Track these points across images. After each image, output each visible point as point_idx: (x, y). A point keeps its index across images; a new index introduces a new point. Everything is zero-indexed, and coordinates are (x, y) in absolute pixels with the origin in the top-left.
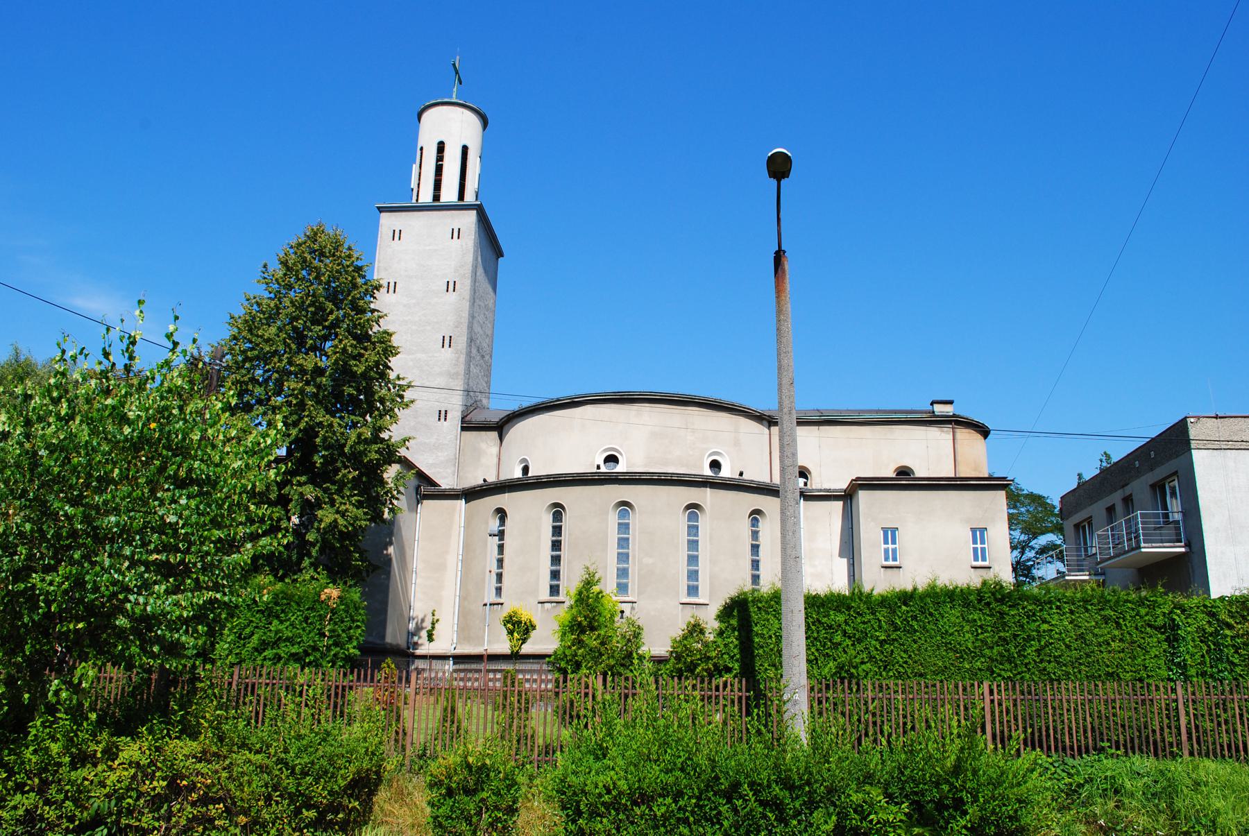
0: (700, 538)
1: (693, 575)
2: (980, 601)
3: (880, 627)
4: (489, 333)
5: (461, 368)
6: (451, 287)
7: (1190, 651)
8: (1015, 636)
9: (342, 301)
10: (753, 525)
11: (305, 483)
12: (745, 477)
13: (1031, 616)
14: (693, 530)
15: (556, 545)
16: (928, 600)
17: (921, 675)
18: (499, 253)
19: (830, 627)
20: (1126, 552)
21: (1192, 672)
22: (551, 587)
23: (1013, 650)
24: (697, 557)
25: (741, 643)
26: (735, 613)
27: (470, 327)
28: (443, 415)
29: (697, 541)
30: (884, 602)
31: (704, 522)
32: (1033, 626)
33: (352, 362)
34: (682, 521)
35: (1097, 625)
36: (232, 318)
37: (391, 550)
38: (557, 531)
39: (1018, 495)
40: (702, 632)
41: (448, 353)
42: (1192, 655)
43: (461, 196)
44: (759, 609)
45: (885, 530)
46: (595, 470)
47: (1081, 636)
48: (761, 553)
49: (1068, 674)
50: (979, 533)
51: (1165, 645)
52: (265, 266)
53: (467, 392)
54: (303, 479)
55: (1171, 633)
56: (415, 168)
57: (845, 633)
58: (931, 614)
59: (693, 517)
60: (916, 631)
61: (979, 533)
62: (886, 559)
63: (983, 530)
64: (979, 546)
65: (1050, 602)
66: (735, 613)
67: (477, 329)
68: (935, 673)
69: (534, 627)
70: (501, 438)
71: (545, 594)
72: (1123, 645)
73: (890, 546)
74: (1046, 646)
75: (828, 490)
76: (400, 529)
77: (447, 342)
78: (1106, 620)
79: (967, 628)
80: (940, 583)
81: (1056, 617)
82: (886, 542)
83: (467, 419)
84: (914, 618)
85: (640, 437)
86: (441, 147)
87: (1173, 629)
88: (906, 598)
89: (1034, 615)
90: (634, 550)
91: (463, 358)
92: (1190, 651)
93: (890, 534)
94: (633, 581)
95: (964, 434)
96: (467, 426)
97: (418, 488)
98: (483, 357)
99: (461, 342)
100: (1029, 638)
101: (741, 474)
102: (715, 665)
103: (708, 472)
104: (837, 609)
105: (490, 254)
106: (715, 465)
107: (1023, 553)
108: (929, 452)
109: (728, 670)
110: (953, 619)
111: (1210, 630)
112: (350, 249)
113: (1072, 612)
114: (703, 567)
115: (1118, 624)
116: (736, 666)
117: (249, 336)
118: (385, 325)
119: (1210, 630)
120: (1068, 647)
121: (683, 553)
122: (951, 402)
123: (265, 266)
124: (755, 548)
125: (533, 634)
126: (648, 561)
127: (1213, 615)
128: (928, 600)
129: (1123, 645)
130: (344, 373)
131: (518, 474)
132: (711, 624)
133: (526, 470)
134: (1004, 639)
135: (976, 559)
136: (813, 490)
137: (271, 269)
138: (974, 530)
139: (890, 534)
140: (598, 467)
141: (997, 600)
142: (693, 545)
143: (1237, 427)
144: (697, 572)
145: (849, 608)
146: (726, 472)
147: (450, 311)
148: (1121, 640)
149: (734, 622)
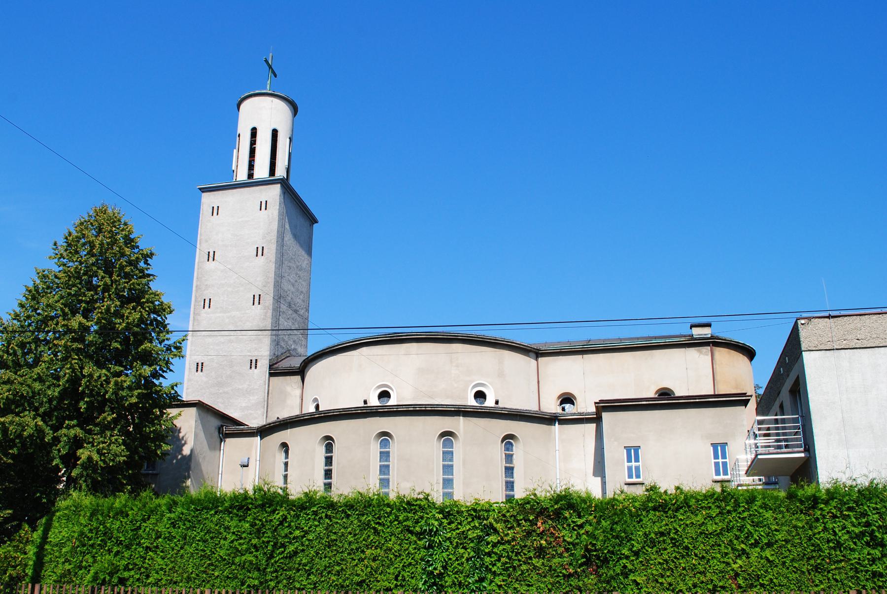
0: (377, 464)
4: (304, 290)
6: (260, 252)
10: (507, 449)
11: (74, 426)
12: (500, 405)
14: (448, 455)
18: (312, 220)
27: (278, 285)
28: (254, 364)
29: (452, 466)
31: (458, 448)
34: (437, 448)
37: (189, 482)
38: (329, 461)
41: (258, 309)
43: (272, 171)
45: (628, 449)
46: (362, 405)
50: (719, 449)
52: (55, 244)
54: (75, 422)
56: (235, 151)
59: (448, 444)
61: (719, 449)
62: (630, 476)
63: (724, 445)
64: (720, 460)
67: (286, 286)
73: (633, 464)
75: (580, 414)
76: (198, 465)
82: (629, 460)
85: (408, 373)
86: (254, 132)
93: (633, 452)
95: (722, 354)
96: (275, 371)
97: (220, 429)
99: (268, 300)
105: (302, 221)
108: (688, 372)
112: (126, 224)
123: (55, 244)
131: (312, 409)
133: (317, 407)
139: (633, 452)
143: (852, 326)
146: (490, 403)
147: (260, 273)
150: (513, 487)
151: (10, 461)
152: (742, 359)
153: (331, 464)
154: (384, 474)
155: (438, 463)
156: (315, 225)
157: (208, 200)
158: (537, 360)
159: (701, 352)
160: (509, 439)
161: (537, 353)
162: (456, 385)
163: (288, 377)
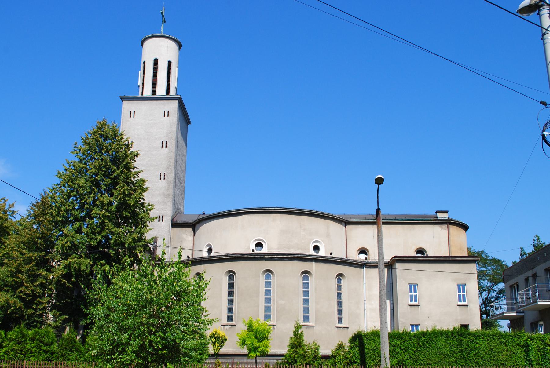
0: (310, 289)
1: (306, 310)
2: (452, 335)
3: (414, 346)
4: (184, 169)
5: (171, 192)
6: (164, 144)
7: (534, 355)
8: (466, 349)
9: (119, 165)
10: (338, 282)
12: (334, 255)
13: (472, 341)
14: (306, 285)
15: (231, 294)
16: (432, 335)
17: (430, 364)
19: (395, 346)
20: (531, 304)
21: (534, 363)
22: (228, 317)
23: (465, 354)
24: (308, 300)
25: (360, 352)
26: (357, 340)
27: (176, 168)
29: (308, 291)
30: (415, 336)
31: (312, 281)
32: (473, 345)
33: (127, 198)
34: (300, 281)
35: (498, 345)
36: (59, 173)
38: (231, 286)
39: (486, 260)
40: (344, 347)
42: (535, 357)
44: (367, 338)
45: (410, 285)
47: (491, 349)
48: (342, 298)
49: (486, 364)
50: (461, 287)
51: (524, 353)
52: (76, 144)
53: (174, 205)
54: (103, 262)
55: (526, 348)
56: (140, 74)
57: (400, 348)
58: (433, 341)
60: (428, 347)
61: (461, 287)
62: (411, 301)
63: (463, 285)
65: (479, 336)
66: (357, 340)
67: (179, 168)
68: (435, 363)
69: (226, 340)
70: (194, 232)
71: (225, 321)
72: (507, 353)
73: (413, 294)
74: (478, 353)
77: (163, 176)
78: (501, 343)
79: (447, 346)
80: (437, 328)
81: (482, 342)
82: (411, 292)
83: (175, 220)
84: (427, 342)
85: (275, 233)
86: (156, 62)
87: (527, 347)
88: (424, 334)
89: (473, 341)
90: (274, 296)
91: (172, 186)
92: (534, 355)
93: (413, 287)
94: (274, 313)
95: (453, 228)
96: (175, 225)
98: (181, 183)
99: (171, 176)
100: (471, 350)
101: (331, 254)
102: (350, 360)
103: (312, 252)
104: (397, 339)
106: (316, 248)
107: (489, 293)
108: (435, 240)
109: (355, 362)
110: (442, 342)
111: (541, 347)
113: (488, 340)
114: (312, 306)
115: (506, 344)
116: (358, 361)
117: (72, 185)
118: (141, 176)
119: (541, 347)
120: (486, 353)
121: (301, 298)
122: (447, 212)
123: (76, 144)
124: (339, 295)
125: (225, 343)
126: (281, 302)
127: (543, 341)
128: (432, 335)
129: (507, 353)
130: (123, 205)
132: (347, 344)
134: (462, 350)
135: (460, 301)
136: (371, 262)
137: (79, 145)
138: (459, 285)
139: (413, 287)
140: (253, 250)
141: (459, 335)
142: (306, 293)
144: (308, 308)
145: (402, 338)
146: (322, 253)
148: (507, 351)
149: (357, 344)
150: (341, 304)
151: (71, 286)
152: (461, 231)
153: (233, 288)
154: (268, 295)
155: (301, 289)
156: (189, 125)
157: (127, 106)
158: (345, 227)
159: (442, 228)
160: (340, 276)
161: (346, 223)
162: (303, 241)
163: (184, 229)
